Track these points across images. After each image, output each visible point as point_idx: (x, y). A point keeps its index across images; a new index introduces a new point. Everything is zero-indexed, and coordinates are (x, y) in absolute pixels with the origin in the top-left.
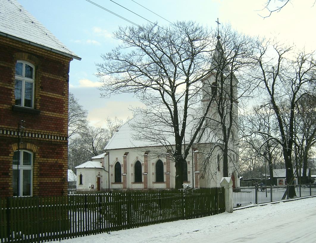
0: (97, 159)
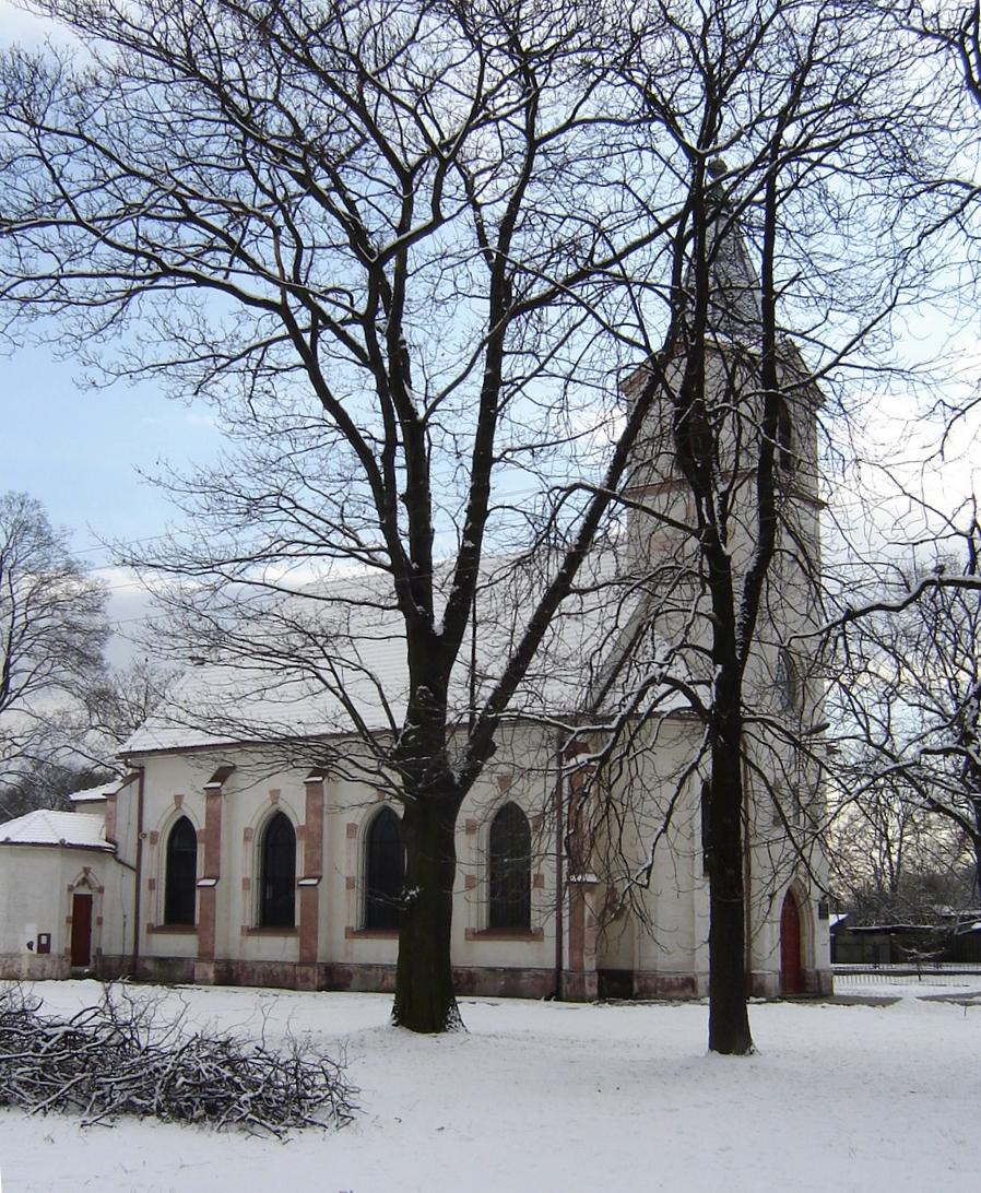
0: (96, 804)
